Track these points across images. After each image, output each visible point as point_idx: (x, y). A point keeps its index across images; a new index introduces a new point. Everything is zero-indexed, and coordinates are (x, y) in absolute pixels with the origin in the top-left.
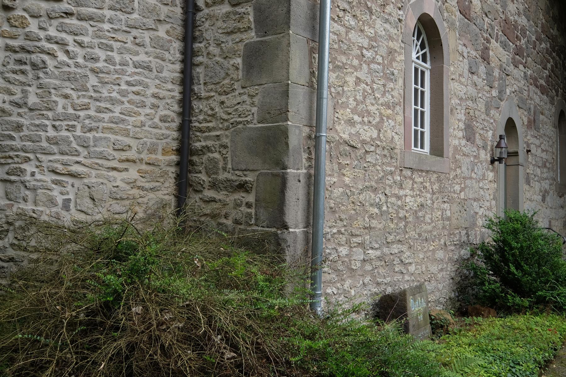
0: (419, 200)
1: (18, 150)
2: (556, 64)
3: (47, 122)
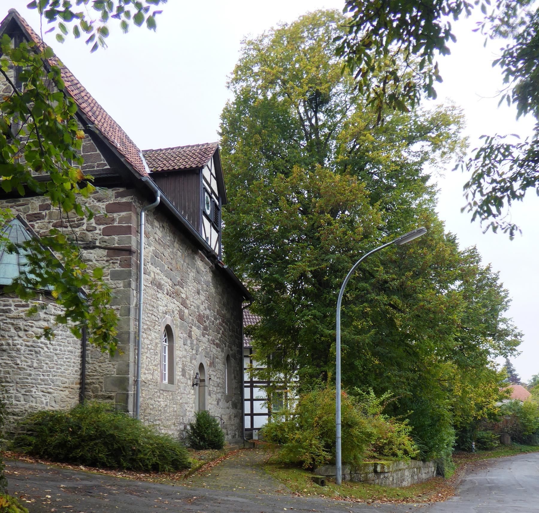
0: (166, 403)
2: (225, 330)
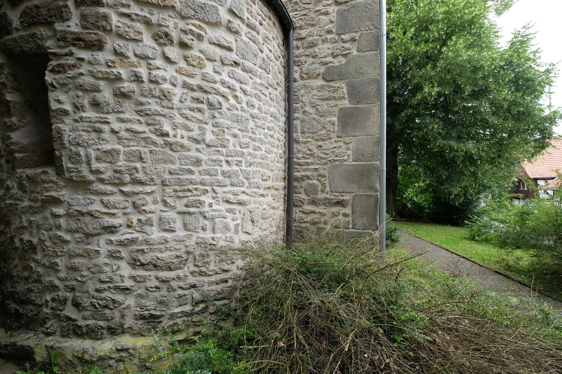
1: (197, 183)
3: (222, 158)
